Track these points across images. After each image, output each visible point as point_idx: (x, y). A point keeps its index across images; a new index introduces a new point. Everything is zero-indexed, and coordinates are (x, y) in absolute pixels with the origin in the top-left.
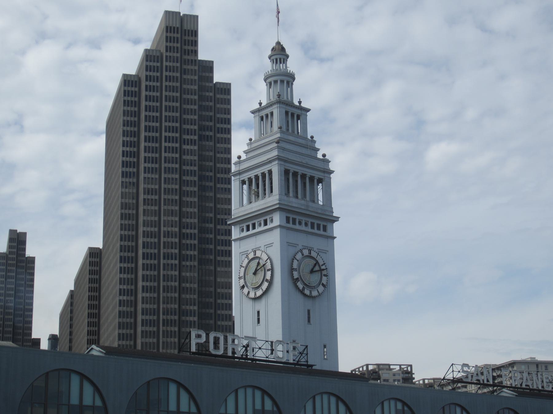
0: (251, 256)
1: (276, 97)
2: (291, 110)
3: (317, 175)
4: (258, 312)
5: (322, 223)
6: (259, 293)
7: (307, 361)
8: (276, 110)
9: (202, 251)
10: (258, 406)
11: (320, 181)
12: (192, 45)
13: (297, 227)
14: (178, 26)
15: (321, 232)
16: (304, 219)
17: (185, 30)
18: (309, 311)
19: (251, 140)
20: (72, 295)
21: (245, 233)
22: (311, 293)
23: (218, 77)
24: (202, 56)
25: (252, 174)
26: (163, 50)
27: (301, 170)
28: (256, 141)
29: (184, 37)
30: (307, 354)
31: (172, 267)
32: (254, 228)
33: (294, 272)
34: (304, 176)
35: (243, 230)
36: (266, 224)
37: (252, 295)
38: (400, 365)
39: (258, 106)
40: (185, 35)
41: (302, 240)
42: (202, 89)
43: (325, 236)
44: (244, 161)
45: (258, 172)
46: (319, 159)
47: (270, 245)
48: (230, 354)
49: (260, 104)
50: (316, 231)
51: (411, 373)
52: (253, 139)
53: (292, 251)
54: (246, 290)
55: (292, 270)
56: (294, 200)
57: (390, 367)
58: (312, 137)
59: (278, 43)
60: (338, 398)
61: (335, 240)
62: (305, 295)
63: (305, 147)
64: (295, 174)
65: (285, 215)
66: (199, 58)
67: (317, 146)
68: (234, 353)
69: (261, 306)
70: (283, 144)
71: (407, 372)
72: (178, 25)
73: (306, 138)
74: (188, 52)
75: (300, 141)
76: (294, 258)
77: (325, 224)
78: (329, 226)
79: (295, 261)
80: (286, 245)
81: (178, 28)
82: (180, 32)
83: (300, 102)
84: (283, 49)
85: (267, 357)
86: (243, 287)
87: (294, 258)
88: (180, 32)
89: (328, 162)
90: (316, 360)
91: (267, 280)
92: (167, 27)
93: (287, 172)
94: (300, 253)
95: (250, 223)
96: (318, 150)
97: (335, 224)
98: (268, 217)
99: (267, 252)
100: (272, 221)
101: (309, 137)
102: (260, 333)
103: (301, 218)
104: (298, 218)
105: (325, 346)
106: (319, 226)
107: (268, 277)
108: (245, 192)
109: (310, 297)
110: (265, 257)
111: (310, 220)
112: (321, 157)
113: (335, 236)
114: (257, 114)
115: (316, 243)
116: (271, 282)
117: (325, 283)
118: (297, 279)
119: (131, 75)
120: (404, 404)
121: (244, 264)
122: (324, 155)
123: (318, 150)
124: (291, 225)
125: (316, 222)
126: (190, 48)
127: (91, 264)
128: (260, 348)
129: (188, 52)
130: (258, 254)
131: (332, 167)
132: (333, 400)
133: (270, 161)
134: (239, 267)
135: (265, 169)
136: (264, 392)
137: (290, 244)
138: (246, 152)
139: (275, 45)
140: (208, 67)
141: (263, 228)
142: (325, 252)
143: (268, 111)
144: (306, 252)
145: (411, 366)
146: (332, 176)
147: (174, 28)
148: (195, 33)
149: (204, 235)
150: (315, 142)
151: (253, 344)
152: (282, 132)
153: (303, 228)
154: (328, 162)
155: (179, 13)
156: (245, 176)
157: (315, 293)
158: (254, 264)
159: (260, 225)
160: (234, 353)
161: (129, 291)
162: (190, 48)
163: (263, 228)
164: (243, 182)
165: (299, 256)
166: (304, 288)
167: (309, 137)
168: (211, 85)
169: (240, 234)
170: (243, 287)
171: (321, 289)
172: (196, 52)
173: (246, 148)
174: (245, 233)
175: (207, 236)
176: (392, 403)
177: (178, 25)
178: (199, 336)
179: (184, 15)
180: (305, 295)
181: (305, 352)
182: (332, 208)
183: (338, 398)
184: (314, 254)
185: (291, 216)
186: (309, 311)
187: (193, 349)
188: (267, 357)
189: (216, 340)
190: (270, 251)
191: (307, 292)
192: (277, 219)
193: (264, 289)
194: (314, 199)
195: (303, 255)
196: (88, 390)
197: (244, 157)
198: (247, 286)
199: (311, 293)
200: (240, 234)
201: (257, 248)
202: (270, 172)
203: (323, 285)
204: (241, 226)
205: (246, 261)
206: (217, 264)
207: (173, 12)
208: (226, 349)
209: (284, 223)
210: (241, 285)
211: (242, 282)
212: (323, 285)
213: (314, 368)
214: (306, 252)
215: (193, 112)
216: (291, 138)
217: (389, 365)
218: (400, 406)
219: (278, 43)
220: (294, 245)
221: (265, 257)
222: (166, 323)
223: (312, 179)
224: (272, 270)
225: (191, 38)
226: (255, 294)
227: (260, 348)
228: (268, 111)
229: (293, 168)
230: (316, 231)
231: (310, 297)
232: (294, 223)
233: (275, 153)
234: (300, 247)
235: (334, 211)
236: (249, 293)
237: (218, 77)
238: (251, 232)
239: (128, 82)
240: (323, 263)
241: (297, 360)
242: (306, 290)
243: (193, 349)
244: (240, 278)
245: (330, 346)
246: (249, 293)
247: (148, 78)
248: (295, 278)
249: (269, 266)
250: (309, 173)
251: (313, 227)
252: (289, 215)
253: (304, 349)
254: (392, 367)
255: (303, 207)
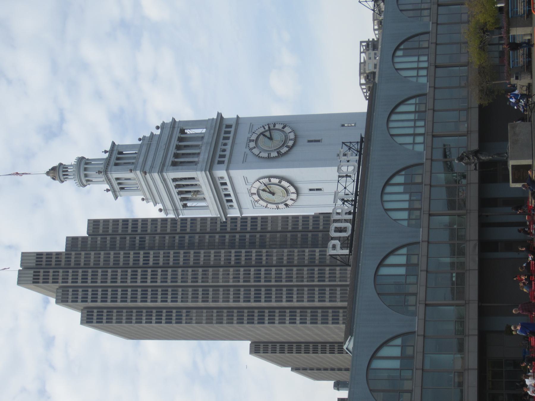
0: (256, 197)
1: (101, 175)
2: (113, 161)
3: (177, 134)
4: (311, 190)
5: (224, 129)
6: (292, 189)
7: (358, 142)
8: (114, 175)
9: (252, 244)
10: (401, 189)
11: (182, 131)
12: (51, 258)
13: (227, 153)
14: (32, 272)
15: (232, 130)
16: (220, 147)
17: (37, 265)
18: (309, 141)
19: (143, 199)
20: (296, 369)
21: (235, 203)
22: (291, 140)
23: (82, 231)
24: (60, 247)
25: (177, 198)
26: (56, 286)
27: (172, 150)
28: (145, 194)
29: (44, 266)
30: (351, 143)
31: (268, 273)
32: (229, 195)
33: (272, 156)
34: (178, 148)
35: (232, 206)
36: (225, 184)
37: (294, 196)
38: (361, 53)
39: (110, 193)
40: (41, 265)
41: (241, 149)
42: (94, 248)
43: (236, 126)
44: (164, 205)
45: (174, 192)
46: (161, 132)
47: (246, 179)
48: (351, 217)
49: (108, 190)
50: (231, 135)
51: (368, 43)
52: (143, 197)
53: (250, 157)
54: (289, 202)
55: (269, 158)
56: (201, 157)
57: (362, 63)
58: (140, 140)
59: (48, 173)
60: (392, 112)
61: (240, 116)
62: (294, 145)
63: (149, 146)
64: (176, 156)
65: (216, 166)
66: (64, 250)
67: (148, 135)
68: (350, 213)
69: (304, 188)
70: (147, 169)
71: (367, 46)
72: (32, 272)
73: (141, 145)
74: (58, 261)
75: (144, 151)
76: (258, 156)
77: (224, 126)
78: (225, 123)
79: (261, 155)
80: (245, 164)
81: (34, 272)
82: (39, 270)
83: (106, 152)
84: (54, 169)
85: (354, 181)
86: (286, 205)
87: (258, 156)
88: (39, 270)
89: (163, 123)
90: (357, 134)
91: (280, 182)
92: (34, 282)
93: (174, 164)
94: (253, 150)
95: (225, 199)
96: (152, 133)
97: (225, 116)
98: (219, 182)
99: (253, 182)
100: (222, 178)
101: (140, 142)
102: (330, 188)
103: (219, 150)
104: (219, 153)
105: (343, 125)
106: (226, 132)
107: (276, 181)
108: (194, 204)
109: (295, 140)
110: (257, 184)
111: (221, 141)
112: (159, 130)
113: (236, 117)
114: (118, 193)
115: (243, 135)
116: (282, 178)
117: (282, 126)
118: (278, 152)
119: (82, 317)
120: (397, 49)
121: (265, 204)
122: (158, 128)
123: (152, 133)
124: (226, 160)
125: (222, 135)
126: (54, 260)
127: (266, 351)
128: (345, 188)
129: (58, 261)
130: (254, 191)
131: (168, 120)
132: (394, 117)
133: (164, 180)
134: (266, 209)
135: (172, 185)
136: (387, 183)
137: (244, 161)
138: (155, 204)
139: (49, 177)
140: (73, 242)
141: (229, 187)
142: (252, 126)
143: (115, 183)
144: (252, 145)
145: (361, 42)
146: (177, 120)
147: (34, 275)
148: (39, 255)
149: (237, 244)
150: (144, 137)
151: (342, 194)
152: (135, 169)
153: (228, 148)
154: (163, 123)
155: (19, 270)
156: (179, 204)
157: (292, 136)
158: (264, 195)
159: (226, 189)
160: (350, 213)
161: (292, 315)
162: (54, 260)
163: (229, 187)
164: (185, 206)
165: (256, 151)
166: (287, 146)
167: (140, 142)
168: (90, 239)
169: (235, 208)
170: (286, 205)
171: (287, 130)
172: (58, 254)
173: (151, 204)
174: (235, 203)
175: (237, 240)
176: (396, 60)
177: (32, 272)
178: (334, 247)
179: (21, 266)
180: (294, 145)
181: (348, 144)
182: (209, 120)
183: (392, 112)
184: (254, 137)
185: (217, 159)
186: (309, 141)
187: (346, 252)
188: (354, 181)
189: (339, 230)
190: (251, 179)
191: (290, 143)
192: (220, 173)
193: (288, 184)
194: (201, 137)
195: (255, 148)
196: (386, 352)
197: (160, 206)
198: (286, 201)
199: (291, 140)
200: (235, 208)
201: (248, 192)
202: (174, 180)
203: (283, 128)
204: (227, 207)
205: (261, 202)
206: (264, 230)
207: (19, 277)
208: (346, 221)
209: (224, 166)
210: (285, 206)
211: (282, 206)
212: (283, 128)
213: (363, 136)
214: (252, 145)
215: (117, 256)
216: (141, 160)
217: (361, 63)
218: (399, 53)
219: (48, 173)
220: (245, 155)
221: (257, 184)
222: (321, 278)
223: (180, 139)
224: (269, 177)
225: (44, 259)
226: (293, 193)
227: (345, 188)
228: (115, 183)
229: (170, 158)
230: (231, 135)
231: (295, 140)
232: (224, 156)
233: (156, 176)
234: (247, 150)
235: (212, 118)
236: (292, 199)
237: (82, 231)
238: (233, 198)
239: (88, 319)
240: (262, 128)
241: (356, 152)
242: (289, 145)
243: (346, 252)
244: (278, 208)
245: (342, 121)
246: (292, 199)
247: (84, 300)
248: (277, 155)
249: (266, 181)
250: (175, 142)
251: (228, 138)
252: (216, 162)
253: (346, 145)
254: (362, 61)
255: (208, 148)
